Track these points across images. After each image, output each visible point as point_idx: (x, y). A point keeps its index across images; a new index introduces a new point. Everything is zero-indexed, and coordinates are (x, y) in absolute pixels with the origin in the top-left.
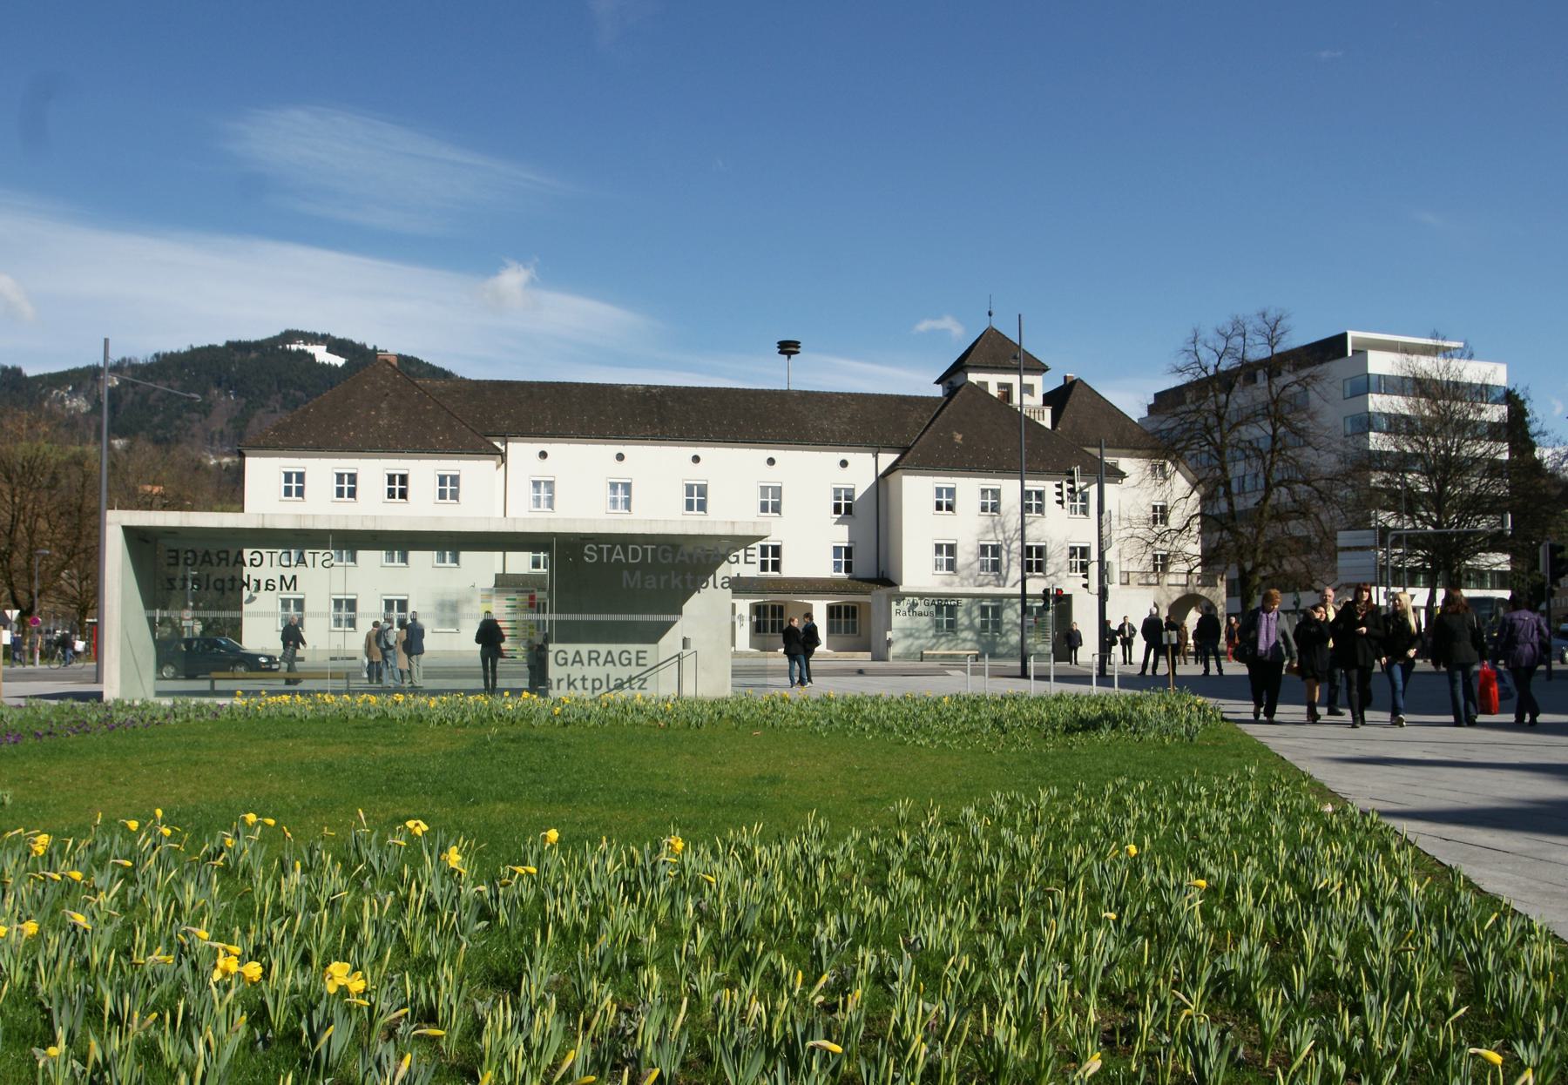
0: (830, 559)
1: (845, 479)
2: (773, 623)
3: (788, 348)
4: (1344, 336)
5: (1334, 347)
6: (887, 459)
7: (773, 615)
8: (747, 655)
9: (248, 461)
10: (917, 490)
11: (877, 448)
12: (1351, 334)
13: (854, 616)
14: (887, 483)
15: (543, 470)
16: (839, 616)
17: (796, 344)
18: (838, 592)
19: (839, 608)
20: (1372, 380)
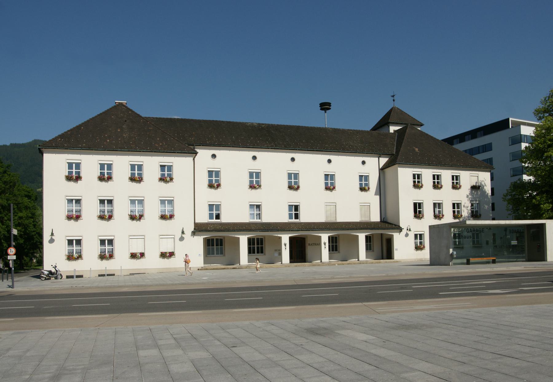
0: (286, 212)
1: (364, 170)
2: (258, 248)
3: (325, 106)
4: (508, 120)
5: (503, 125)
6: (384, 160)
7: (258, 244)
8: (366, 262)
9: (45, 155)
10: (405, 174)
11: (380, 155)
12: (510, 119)
13: (221, 245)
14: (384, 173)
15: (214, 165)
16: (213, 245)
17: (329, 104)
18: (209, 231)
19: (254, 239)
20: (522, 137)
